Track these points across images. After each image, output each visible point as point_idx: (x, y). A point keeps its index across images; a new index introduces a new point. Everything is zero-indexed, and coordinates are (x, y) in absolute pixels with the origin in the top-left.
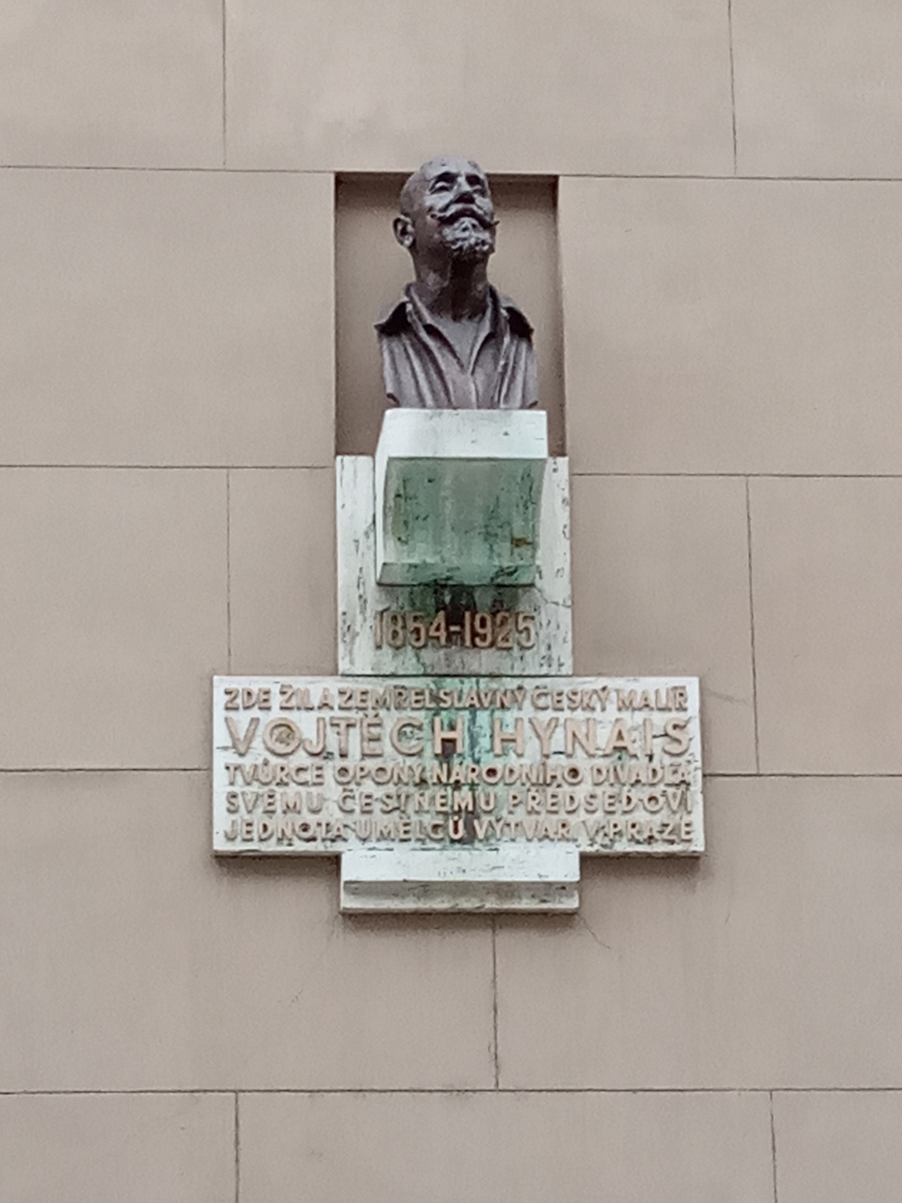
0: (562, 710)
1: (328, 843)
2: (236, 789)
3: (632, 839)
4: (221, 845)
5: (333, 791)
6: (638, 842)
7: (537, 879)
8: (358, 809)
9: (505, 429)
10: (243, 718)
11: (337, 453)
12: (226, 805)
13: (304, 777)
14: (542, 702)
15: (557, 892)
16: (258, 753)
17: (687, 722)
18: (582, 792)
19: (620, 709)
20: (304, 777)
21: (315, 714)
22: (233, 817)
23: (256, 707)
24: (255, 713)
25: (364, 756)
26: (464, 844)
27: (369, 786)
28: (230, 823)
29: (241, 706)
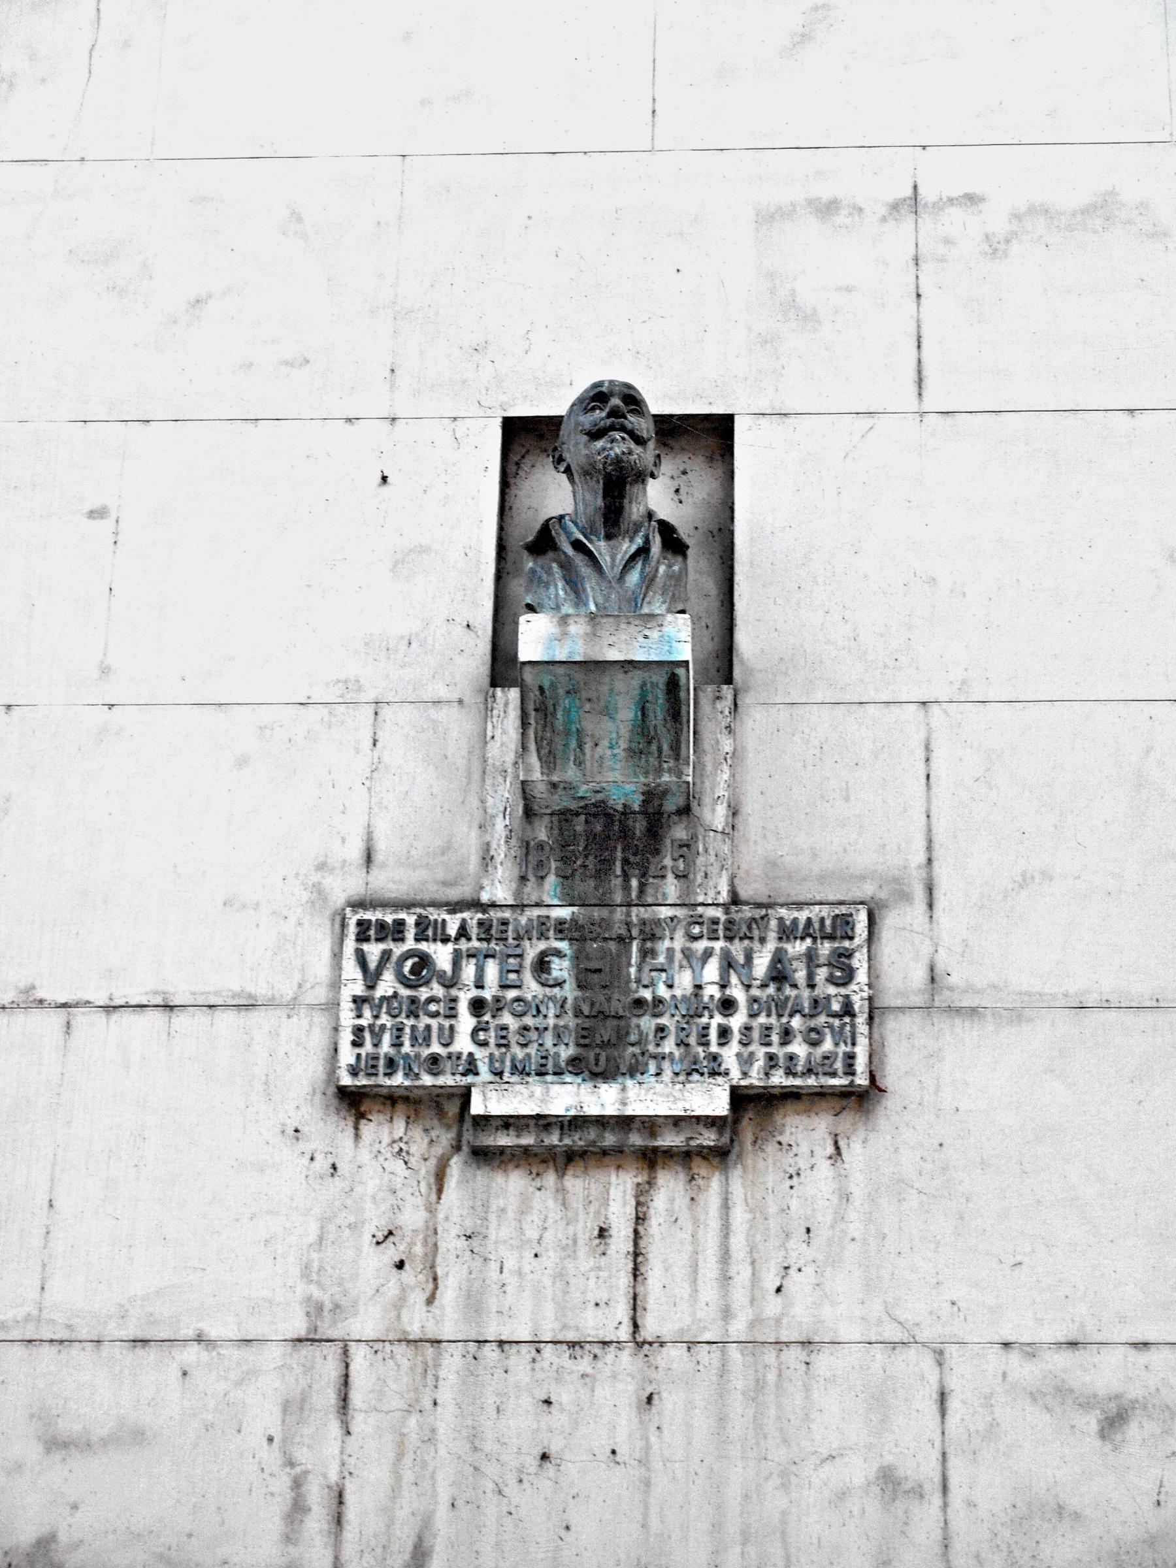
0: (718, 939)
1: (458, 1077)
2: (364, 1022)
3: (790, 1072)
4: (346, 1080)
5: (466, 1022)
6: (795, 1075)
7: (683, 1113)
8: (492, 1041)
9: (700, 530)
10: (373, 950)
11: (494, 684)
12: (352, 1038)
13: (433, 1007)
14: (696, 930)
15: (782, 1174)
16: (387, 985)
17: (853, 951)
18: (737, 1022)
19: (780, 939)
20: (433, 1007)
21: (450, 947)
22: (358, 1050)
23: (390, 938)
24: (389, 945)
25: (504, 987)
26: (539, 1117)
27: (507, 1019)
28: (355, 1056)
29: (373, 937)
